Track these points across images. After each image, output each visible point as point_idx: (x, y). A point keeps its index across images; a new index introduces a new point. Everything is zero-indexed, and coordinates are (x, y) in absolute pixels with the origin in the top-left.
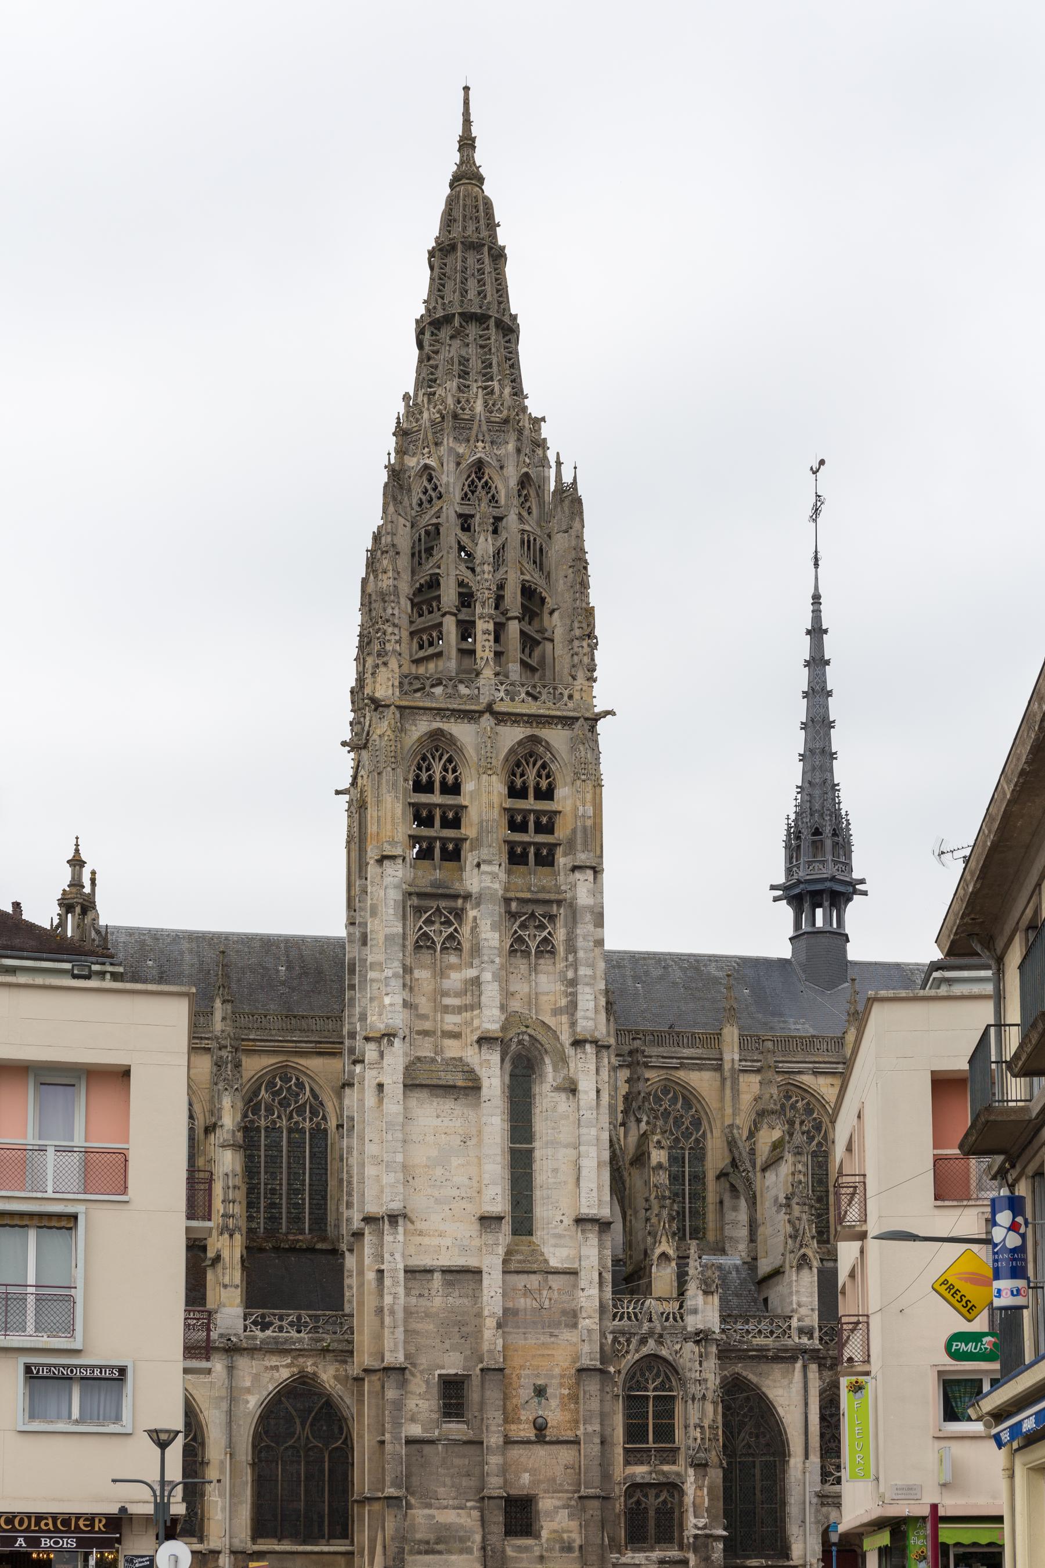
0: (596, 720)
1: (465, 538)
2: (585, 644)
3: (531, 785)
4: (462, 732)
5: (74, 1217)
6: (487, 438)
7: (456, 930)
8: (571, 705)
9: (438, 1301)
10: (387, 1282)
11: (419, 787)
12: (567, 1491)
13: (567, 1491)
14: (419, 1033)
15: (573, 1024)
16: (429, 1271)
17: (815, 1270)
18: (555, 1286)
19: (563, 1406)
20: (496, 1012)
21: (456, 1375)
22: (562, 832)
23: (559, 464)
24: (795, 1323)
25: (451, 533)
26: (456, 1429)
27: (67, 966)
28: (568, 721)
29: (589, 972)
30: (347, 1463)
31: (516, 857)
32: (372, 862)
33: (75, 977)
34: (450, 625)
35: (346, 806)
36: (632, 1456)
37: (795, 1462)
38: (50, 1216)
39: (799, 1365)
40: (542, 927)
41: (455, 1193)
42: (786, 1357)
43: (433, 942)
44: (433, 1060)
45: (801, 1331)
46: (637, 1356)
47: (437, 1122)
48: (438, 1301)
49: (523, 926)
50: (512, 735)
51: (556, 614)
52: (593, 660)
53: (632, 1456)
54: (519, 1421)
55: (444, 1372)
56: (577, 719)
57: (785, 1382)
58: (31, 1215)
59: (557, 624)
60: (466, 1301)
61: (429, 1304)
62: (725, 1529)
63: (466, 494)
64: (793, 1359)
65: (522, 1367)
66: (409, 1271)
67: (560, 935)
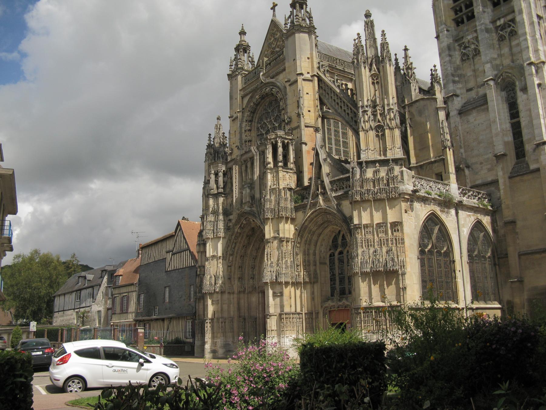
7: (513, 27)
43: (505, 37)
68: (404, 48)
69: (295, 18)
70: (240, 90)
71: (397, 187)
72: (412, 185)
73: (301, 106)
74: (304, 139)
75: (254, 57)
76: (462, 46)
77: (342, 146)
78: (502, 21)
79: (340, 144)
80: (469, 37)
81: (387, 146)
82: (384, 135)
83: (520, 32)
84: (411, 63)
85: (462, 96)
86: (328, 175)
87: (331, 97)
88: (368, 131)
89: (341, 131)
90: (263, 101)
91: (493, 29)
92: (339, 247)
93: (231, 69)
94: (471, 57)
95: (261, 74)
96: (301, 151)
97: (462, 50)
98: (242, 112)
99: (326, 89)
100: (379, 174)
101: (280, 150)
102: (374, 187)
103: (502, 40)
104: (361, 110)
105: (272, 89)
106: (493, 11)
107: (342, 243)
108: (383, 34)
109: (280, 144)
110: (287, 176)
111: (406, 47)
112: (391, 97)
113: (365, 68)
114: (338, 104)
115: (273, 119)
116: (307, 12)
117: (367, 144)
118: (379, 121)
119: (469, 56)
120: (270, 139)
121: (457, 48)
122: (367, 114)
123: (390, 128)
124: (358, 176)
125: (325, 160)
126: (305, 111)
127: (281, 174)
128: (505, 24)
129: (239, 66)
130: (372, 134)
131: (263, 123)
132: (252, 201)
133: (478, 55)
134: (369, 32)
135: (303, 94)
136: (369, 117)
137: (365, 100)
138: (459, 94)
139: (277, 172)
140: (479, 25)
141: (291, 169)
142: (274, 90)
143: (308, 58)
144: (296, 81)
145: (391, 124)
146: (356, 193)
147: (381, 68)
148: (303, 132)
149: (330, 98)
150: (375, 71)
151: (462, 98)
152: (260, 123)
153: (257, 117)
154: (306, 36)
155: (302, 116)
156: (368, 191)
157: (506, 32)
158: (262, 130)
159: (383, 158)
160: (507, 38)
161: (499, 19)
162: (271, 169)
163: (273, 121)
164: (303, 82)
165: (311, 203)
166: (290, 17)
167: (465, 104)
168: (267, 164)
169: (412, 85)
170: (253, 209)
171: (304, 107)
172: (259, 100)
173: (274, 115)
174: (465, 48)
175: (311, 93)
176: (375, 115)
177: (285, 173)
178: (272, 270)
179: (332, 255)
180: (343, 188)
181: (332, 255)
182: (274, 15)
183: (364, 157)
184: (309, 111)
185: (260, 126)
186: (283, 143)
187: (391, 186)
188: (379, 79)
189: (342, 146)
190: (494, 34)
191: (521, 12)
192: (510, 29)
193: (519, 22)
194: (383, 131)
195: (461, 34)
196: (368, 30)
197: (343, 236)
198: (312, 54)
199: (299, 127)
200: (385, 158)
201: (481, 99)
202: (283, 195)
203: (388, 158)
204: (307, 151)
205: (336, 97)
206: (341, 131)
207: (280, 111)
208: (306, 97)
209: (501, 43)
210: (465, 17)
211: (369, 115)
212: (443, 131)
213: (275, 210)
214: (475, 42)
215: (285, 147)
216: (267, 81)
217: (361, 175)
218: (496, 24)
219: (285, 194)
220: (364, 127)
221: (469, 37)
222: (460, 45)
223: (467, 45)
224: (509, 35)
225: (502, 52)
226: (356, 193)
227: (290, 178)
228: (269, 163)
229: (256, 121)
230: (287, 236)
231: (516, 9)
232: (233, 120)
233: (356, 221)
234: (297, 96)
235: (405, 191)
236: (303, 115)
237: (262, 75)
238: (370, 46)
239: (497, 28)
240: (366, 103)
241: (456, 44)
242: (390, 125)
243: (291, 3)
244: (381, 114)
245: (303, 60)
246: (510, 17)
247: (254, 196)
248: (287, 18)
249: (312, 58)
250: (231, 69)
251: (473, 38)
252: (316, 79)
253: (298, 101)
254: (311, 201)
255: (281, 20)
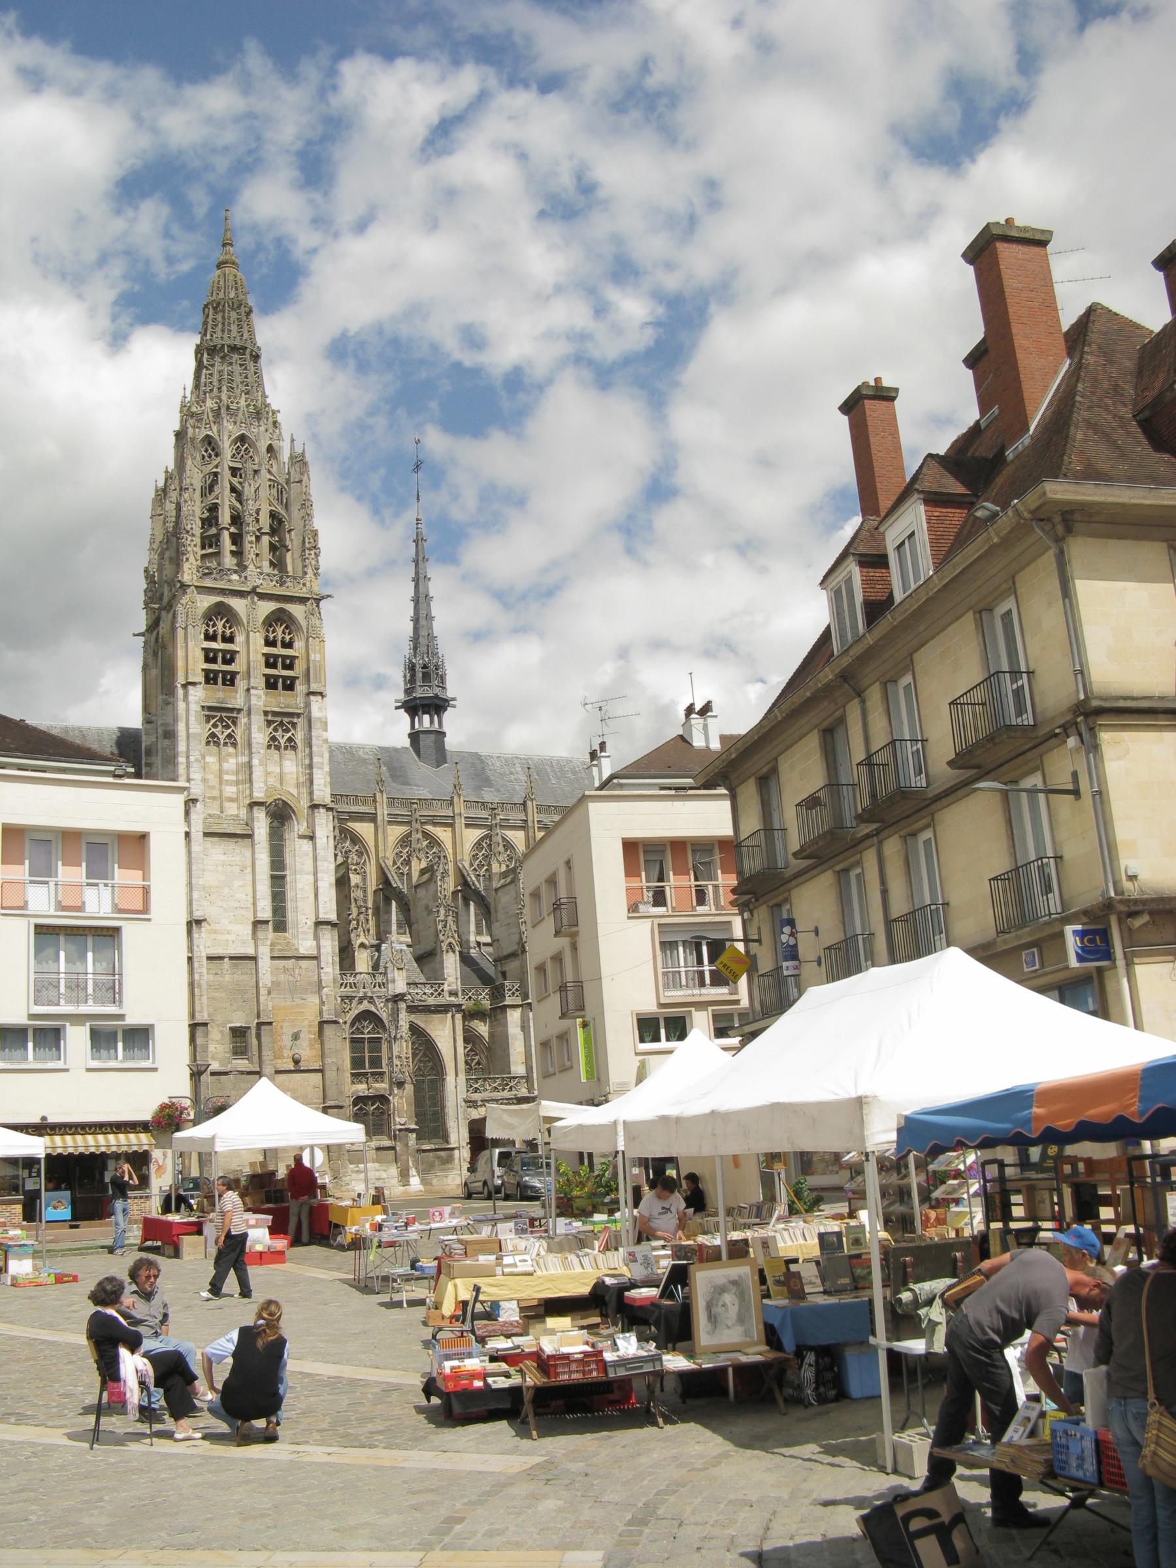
0: (320, 600)
1: (235, 481)
2: (312, 552)
3: (279, 638)
4: (238, 604)
5: (117, 930)
6: (248, 422)
8: (304, 589)
9: (227, 978)
10: (196, 965)
11: (210, 637)
12: (315, 1103)
13: (315, 1103)
14: (209, 798)
15: (311, 793)
16: (221, 958)
17: (457, 953)
18: (303, 967)
19: (311, 1046)
20: (262, 785)
21: (241, 1027)
22: (298, 670)
23: (293, 441)
24: (446, 987)
25: (226, 477)
26: (242, 1064)
27: (112, 768)
28: (303, 600)
29: (320, 760)
30: (490, 1073)
31: (271, 684)
32: (179, 686)
33: (116, 776)
34: (226, 538)
35: (143, 645)
36: (357, 1077)
37: (450, 1079)
38: (102, 928)
39: (450, 1015)
40: (287, 731)
41: (237, 905)
42: (443, 1009)
43: (218, 738)
44: (219, 817)
45: (451, 994)
46: (357, 1012)
47: (224, 858)
48: (227, 978)
49: (275, 730)
50: (267, 607)
51: (293, 533)
52: (318, 562)
53: (357, 1077)
54: (282, 1057)
55: (233, 1025)
56: (308, 599)
57: (441, 1027)
58: (90, 928)
59: (293, 540)
60: (245, 977)
61: (222, 979)
62: (416, 1124)
63: (234, 455)
64: (446, 1011)
65: (283, 1020)
66: (210, 958)
67: (299, 737)
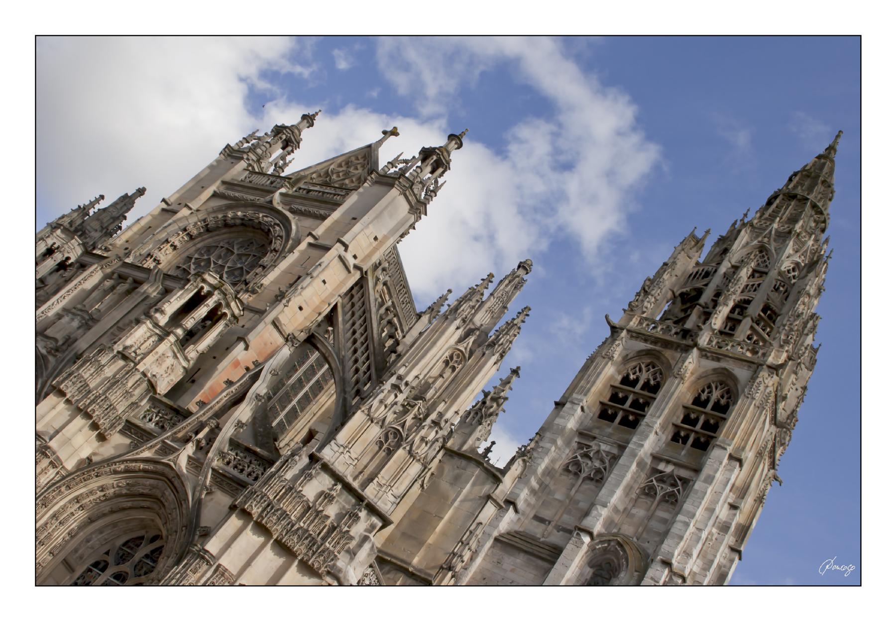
7: (678, 491)
43: (656, 494)
68: (515, 368)
69: (414, 168)
70: (224, 183)
71: (336, 556)
72: (360, 576)
73: (299, 287)
74: (251, 337)
75: (290, 165)
76: (582, 449)
77: (285, 412)
78: (669, 469)
79: (285, 407)
80: (604, 447)
81: (379, 476)
82: (390, 453)
83: (687, 506)
84: (506, 399)
85: (522, 518)
86: (240, 424)
87: (353, 324)
88: (372, 422)
89: (306, 389)
90: (241, 228)
91: (648, 466)
92: (128, 564)
93: (240, 144)
94: (583, 475)
95: (283, 190)
96: (228, 349)
97: (577, 454)
98: (192, 213)
99: (357, 307)
100: (326, 505)
101: (202, 311)
102: (300, 519)
103: (647, 495)
104: (393, 380)
105: (275, 224)
106: (667, 445)
107: (140, 561)
108: (525, 311)
109: (211, 302)
110: (170, 361)
111: (518, 368)
112: (454, 408)
113: (458, 328)
114: (355, 342)
115: (229, 267)
116: (436, 182)
117: (353, 441)
118: (403, 425)
119: (580, 471)
120: (204, 281)
121: (575, 445)
122: (396, 396)
123: (410, 452)
124: (289, 475)
125: (258, 397)
126: (295, 301)
127: (164, 347)
128: (671, 475)
129: (259, 151)
130: (375, 432)
131: (206, 257)
132: (63, 344)
133: (594, 482)
134: (507, 290)
135: (318, 276)
136: (396, 403)
137: (414, 373)
138: (520, 511)
139: (161, 339)
140: (635, 443)
141: (186, 359)
142: (277, 228)
143: (376, 239)
144: (327, 249)
145: (418, 447)
146: (262, 498)
147: (478, 353)
148: (261, 326)
149: (351, 322)
150: (466, 349)
151: (519, 519)
152: (202, 255)
153: (206, 242)
154: (405, 207)
155: (284, 301)
156: (285, 515)
157: (662, 488)
158: (193, 267)
159: (356, 485)
160: (658, 497)
161: (668, 462)
162: (156, 325)
163: (226, 269)
164: (337, 259)
165: (163, 442)
166: (406, 161)
167: (516, 532)
168: (157, 311)
169: (480, 427)
170: (51, 358)
171: (300, 294)
172: (238, 222)
173: (236, 264)
174: (586, 456)
175: (330, 287)
176: (406, 408)
177: (170, 354)
178: (97, 407)
179: (101, 566)
180: (242, 471)
181: (101, 566)
182: (380, 142)
183: (327, 454)
184: (301, 308)
185: (196, 259)
186: (218, 306)
187: (327, 544)
188: (460, 366)
189: (285, 412)
190: (643, 475)
191: (710, 480)
192: (671, 490)
193: (697, 491)
194: (398, 446)
195: (595, 433)
196: (507, 286)
197: (159, 550)
198: (386, 238)
199: (261, 313)
200: (360, 491)
201: (547, 548)
202: (130, 384)
203: (363, 494)
204: (237, 360)
205: (361, 330)
206: (306, 389)
207: (253, 266)
208: (318, 282)
209: (643, 497)
210: (620, 415)
211: (397, 400)
212: (469, 538)
213: (89, 392)
214: (607, 461)
215: (213, 317)
216: (280, 208)
217: (296, 478)
218: (658, 465)
219: (137, 384)
220: (373, 409)
221: (604, 447)
222: (581, 446)
223: (591, 455)
224: (664, 496)
225: (634, 511)
226: (262, 498)
227: (169, 371)
228: (162, 312)
229: (199, 246)
230: (62, 455)
231: (706, 471)
232: (163, 210)
233: (213, 546)
234: (305, 268)
235: (341, 575)
236: (288, 302)
237: (281, 194)
238: (490, 310)
239: (655, 471)
240: (409, 378)
241: (576, 439)
242: (414, 448)
243: (426, 147)
244: (415, 418)
245: (367, 231)
246: (684, 473)
247: (76, 340)
248: (401, 158)
249: (382, 243)
250: (240, 144)
251: (608, 453)
252: (357, 275)
253: (299, 277)
254: (167, 438)
255: (384, 157)
